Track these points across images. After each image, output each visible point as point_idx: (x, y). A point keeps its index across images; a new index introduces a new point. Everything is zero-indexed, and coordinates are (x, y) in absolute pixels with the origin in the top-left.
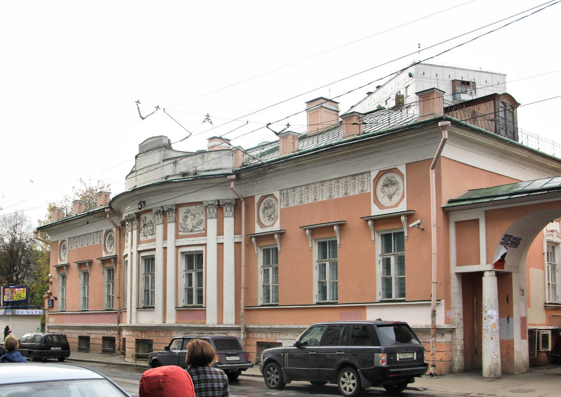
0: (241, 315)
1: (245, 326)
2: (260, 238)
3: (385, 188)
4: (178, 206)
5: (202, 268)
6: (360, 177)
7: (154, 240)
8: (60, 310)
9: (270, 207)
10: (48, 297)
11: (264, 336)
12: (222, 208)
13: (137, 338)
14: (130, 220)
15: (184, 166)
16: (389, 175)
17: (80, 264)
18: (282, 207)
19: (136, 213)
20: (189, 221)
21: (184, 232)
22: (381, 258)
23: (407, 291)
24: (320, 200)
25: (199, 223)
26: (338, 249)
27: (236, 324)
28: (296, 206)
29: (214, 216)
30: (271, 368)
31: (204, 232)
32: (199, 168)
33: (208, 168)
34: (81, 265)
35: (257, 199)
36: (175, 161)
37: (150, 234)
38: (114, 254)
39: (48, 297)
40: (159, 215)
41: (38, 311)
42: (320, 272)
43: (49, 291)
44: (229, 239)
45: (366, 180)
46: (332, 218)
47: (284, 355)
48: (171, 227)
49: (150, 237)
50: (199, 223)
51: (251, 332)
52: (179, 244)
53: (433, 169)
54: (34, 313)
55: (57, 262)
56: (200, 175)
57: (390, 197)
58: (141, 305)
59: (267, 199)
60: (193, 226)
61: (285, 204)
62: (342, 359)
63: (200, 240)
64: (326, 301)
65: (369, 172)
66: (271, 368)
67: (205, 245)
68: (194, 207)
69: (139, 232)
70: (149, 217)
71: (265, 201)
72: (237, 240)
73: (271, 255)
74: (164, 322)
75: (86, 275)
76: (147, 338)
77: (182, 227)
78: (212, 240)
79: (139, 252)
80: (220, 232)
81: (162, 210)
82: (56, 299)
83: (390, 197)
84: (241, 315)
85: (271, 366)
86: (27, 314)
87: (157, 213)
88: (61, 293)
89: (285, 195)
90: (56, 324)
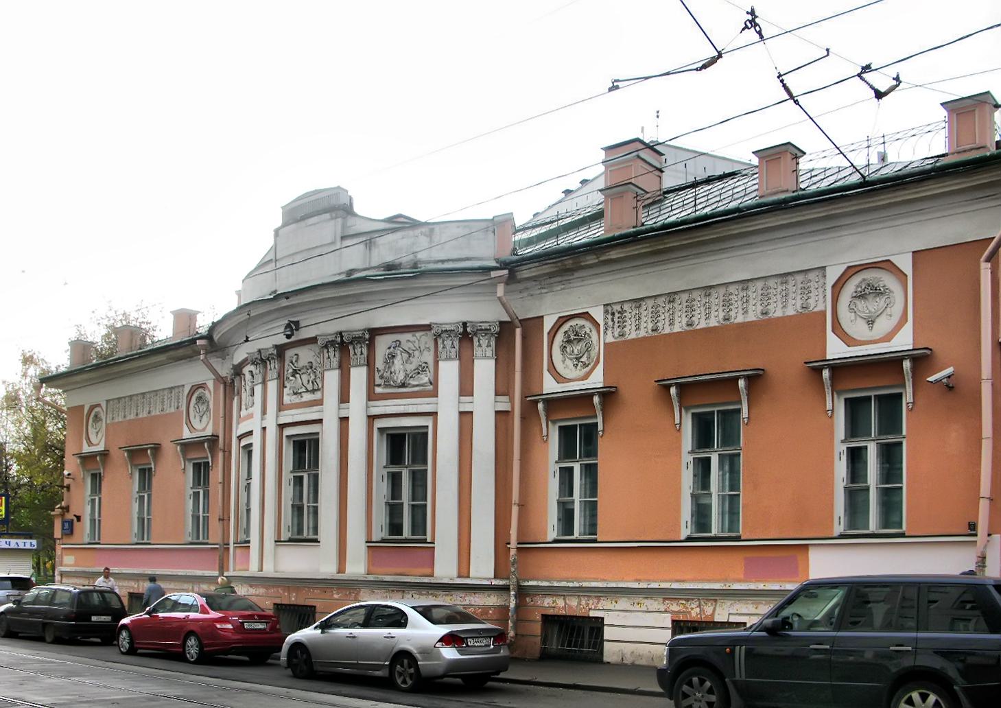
0: (512, 559)
1: (518, 582)
2: (555, 404)
3: (857, 302)
4: (374, 332)
5: (425, 462)
6: (800, 278)
7: (320, 402)
8: (87, 540)
9: (580, 340)
10: (62, 515)
11: (560, 602)
12: (472, 340)
13: (278, 601)
14: (261, 360)
15: (385, 252)
16: (869, 275)
17: (132, 451)
18: (610, 339)
19: (276, 347)
20: (398, 363)
21: (386, 386)
22: (690, 458)
23: (101, 538)
24: (703, 325)
25: (421, 369)
26: (599, 439)
27: (496, 577)
28: (644, 338)
29: (453, 354)
30: (695, 679)
31: (431, 387)
32: (421, 256)
33: (443, 256)
34: (135, 453)
35: (548, 324)
36: (369, 239)
37: (308, 391)
38: (209, 432)
39: (62, 515)
40: (331, 350)
41: (28, 541)
42: (561, 483)
43: (63, 504)
44: (484, 403)
45: (813, 285)
46: (735, 362)
47: (733, 652)
48: (358, 376)
49: (307, 397)
50: (421, 369)
51: (529, 595)
52: (375, 411)
53: (988, 260)
54: (21, 546)
55: (81, 447)
56: (423, 269)
57: (871, 322)
58: (285, 535)
59: (573, 323)
60: (407, 375)
61: (616, 334)
62: (908, 662)
63: (423, 405)
64: (403, 537)
65: (824, 268)
66: (695, 679)
67: (434, 414)
68: (408, 336)
69: (282, 387)
70: (306, 355)
71: (566, 327)
72: (501, 407)
73: (580, 442)
74: (341, 569)
75: (146, 476)
76: (301, 602)
77: (382, 377)
78: (447, 404)
79: (282, 427)
80: (466, 389)
81: (339, 340)
82: (79, 518)
83: (871, 322)
84: (512, 559)
85: (694, 674)
86: (7, 546)
87: (326, 346)
88: (88, 508)
89: (617, 315)
90: (79, 569)
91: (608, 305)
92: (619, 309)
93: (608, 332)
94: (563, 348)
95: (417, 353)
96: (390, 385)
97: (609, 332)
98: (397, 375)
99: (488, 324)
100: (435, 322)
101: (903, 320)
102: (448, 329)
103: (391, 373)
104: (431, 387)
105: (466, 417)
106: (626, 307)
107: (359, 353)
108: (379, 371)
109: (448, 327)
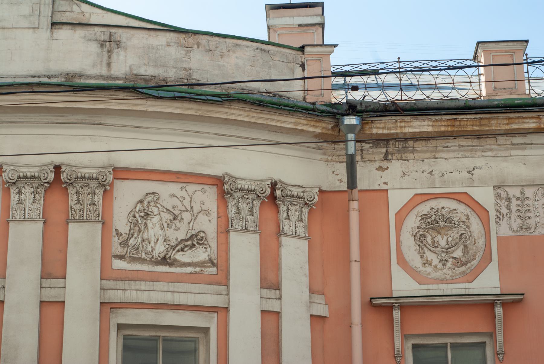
4: (121, 173)
18: (505, 231)
25: (195, 240)
50: (195, 240)
71: (424, 208)
89: (514, 202)
91: (499, 187)
92: (518, 195)
93: (501, 222)
94: (420, 239)
95: (187, 216)
97: (503, 223)
98: (152, 244)
99: (300, 190)
100: (65, 162)
101: (401, 217)
103: (143, 241)
104: (215, 269)
105: (271, 319)
106: (529, 192)
108: (118, 234)
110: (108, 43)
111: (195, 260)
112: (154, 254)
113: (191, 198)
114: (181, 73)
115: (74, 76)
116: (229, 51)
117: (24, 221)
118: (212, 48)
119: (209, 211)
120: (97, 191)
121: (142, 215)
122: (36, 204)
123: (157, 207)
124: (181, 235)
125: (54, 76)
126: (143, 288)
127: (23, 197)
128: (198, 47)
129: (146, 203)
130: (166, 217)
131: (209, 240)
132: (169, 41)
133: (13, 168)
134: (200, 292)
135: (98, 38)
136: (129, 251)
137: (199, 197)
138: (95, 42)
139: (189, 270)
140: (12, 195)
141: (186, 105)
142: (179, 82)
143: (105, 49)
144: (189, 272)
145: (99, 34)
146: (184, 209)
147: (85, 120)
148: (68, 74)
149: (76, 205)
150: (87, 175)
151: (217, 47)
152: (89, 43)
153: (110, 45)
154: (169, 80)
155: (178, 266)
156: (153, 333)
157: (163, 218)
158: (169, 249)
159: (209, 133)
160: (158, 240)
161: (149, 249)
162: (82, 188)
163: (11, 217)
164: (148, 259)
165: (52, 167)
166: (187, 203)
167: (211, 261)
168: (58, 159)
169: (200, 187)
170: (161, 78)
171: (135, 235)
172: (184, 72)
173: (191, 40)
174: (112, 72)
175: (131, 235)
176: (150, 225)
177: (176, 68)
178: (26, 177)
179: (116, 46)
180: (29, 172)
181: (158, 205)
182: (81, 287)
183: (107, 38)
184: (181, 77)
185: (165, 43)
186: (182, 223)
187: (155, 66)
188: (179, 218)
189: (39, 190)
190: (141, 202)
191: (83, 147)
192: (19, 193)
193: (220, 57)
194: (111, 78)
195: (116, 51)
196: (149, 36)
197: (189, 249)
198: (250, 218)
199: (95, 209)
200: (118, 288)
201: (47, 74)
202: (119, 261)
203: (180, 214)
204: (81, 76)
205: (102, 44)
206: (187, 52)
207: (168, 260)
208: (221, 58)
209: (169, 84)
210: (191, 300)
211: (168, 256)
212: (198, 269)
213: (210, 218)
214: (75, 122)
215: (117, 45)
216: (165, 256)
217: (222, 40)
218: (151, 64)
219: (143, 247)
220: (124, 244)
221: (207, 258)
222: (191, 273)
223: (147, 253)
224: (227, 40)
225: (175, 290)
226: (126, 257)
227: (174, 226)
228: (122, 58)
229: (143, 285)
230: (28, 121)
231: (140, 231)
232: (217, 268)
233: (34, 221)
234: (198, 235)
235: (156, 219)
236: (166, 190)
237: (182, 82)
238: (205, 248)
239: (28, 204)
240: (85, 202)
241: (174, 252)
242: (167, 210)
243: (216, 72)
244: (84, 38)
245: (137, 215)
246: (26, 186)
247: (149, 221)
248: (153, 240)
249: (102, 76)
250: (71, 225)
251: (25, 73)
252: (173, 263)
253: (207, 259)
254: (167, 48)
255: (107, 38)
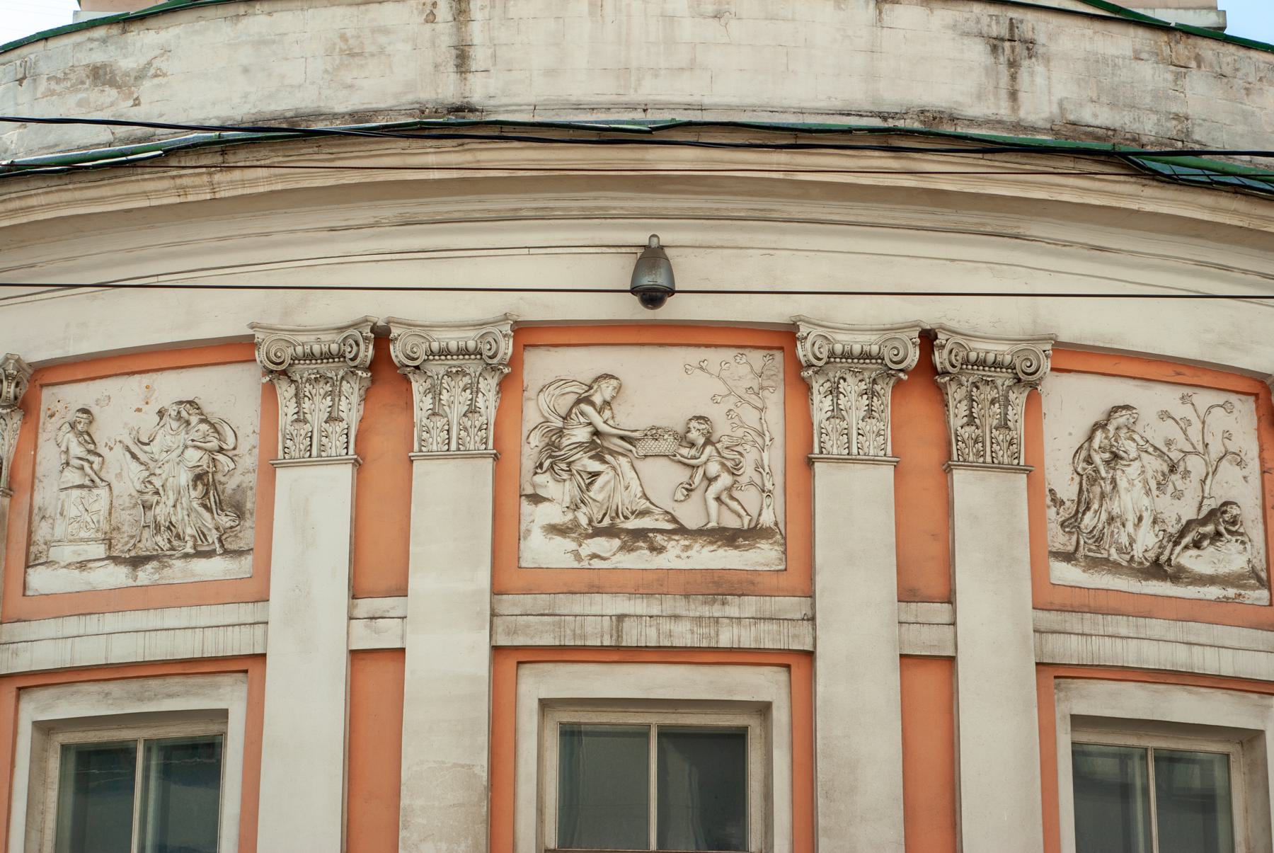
80: (376, 569)
95: (1196, 465)
96: (1107, 561)
98: (1130, 527)
102: (453, 346)
103: (1111, 519)
104: (1264, 594)
105: (375, 667)
107: (455, 413)
109: (453, 339)
110: (1007, 44)
111: (1223, 570)
112: (1135, 553)
113: (1204, 423)
114: (1168, 124)
115: (938, 117)
116: (1261, 79)
117: (848, 459)
118: (1227, 70)
119: (1242, 455)
120: (1012, 396)
121: (1102, 455)
122: (874, 421)
123: (1134, 440)
124: (1189, 513)
125: (894, 116)
126: (1124, 632)
127: (842, 401)
128: (1199, 67)
129: (1111, 428)
130: (1155, 465)
131: (1248, 523)
132: (1138, 47)
133: (820, 331)
134: (1242, 646)
135: (985, 30)
136: (1082, 542)
137: (1219, 420)
138: (978, 40)
139: (1213, 592)
140: (817, 398)
141: (1226, 202)
142: (1166, 145)
143: (1002, 59)
144: (1213, 598)
145: (985, 20)
146: (1188, 448)
147: (983, 224)
148: (922, 112)
149: (967, 429)
150: (991, 358)
151: (1237, 70)
152: (967, 41)
153: (1013, 49)
154: (1144, 140)
155: (1190, 584)
156: (1131, 741)
157: (1148, 466)
158: (1164, 542)
159: (1245, 272)
160: (1140, 519)
161: (1124, 540)
162: (978, 388)
163: (816, 450)
164: (1125, 564)
165: (917, 334)
166: (1195, 433)
167: (1254, 573)
168: (928, 313)
169: (1220, 398)
170: (1128, 136)
171: (1095, 506)
172: (1174, 122)
173: (1183, 49)
174: (1022, 114)
175: (1083, 504)
176: (1122, 483)
177: (1157, 112)
178: (848, 355)
179: (1025, 53)
180: (858, 342)
181: (1136, 437)
182: (991, 624)
183: (1005, 32)
184: (1169, 135)
185: (1129, 53)
186: (1187, 481)
187: (1113, 105)
188: (1181, 469)
189: (877, 388)
190: (1098, 426)
191: (985, 289)
192: (834, 391)
193: (1243, 92)
194: (1017, 126)
195: (1025, 63)
196: (1095, 33)
197: (1211, 543)
198: (1000, 435)
199: (1008, 438)
200: (1069, 629)
201: (876, 109)
202: (1064, 564)
203: (1183, 459)
204: (953, 119)
205: (995, 45)
206: (1177, 77)
207: (1166, 568)
208: (1248, 95)
209: (1148, 149)
210: (1226, 664)
211: (1163, 558)
212: (1231, 592)
213: (1245, 472)
214: (960, 227)
215: (1028, 49)
216: (1158, 558)
217: (1242, 53)
218: (1104, 99)
219: (1112, 535)
220: (1071, 524)
221: (1245, 565)
222: (1218, 601)
223: (1120, 551)
224: (1254, 54)
225: (1193, 639)
226: (1078, 555)
227: (1170, 489)
228: (1040, 81)
229: (1122, 625)
230: (852, 219)
231: (1103, 496)
232: (1270, 590)
233: (874, 461)
234: (1225, 512)
235: (1133, 470)
236: (1152, 400)
237: (1172, 145)
238: (1243, 543)
239: (855, 417)
240: (989, 421)
241: (1178, 549)
242: (1156, 448)
243: (1240, 128)
244: (954, 27)
245: (1097, 458)
246: (848, 376)
247: (1119, 473)
248: (1131, 519)
249: (1000, 122)
250: (958, 475)
251: (822, 104)
252: (1178, 575)
253: (1247, 568)
254: (1135, 64)
255: (1005, 32)
